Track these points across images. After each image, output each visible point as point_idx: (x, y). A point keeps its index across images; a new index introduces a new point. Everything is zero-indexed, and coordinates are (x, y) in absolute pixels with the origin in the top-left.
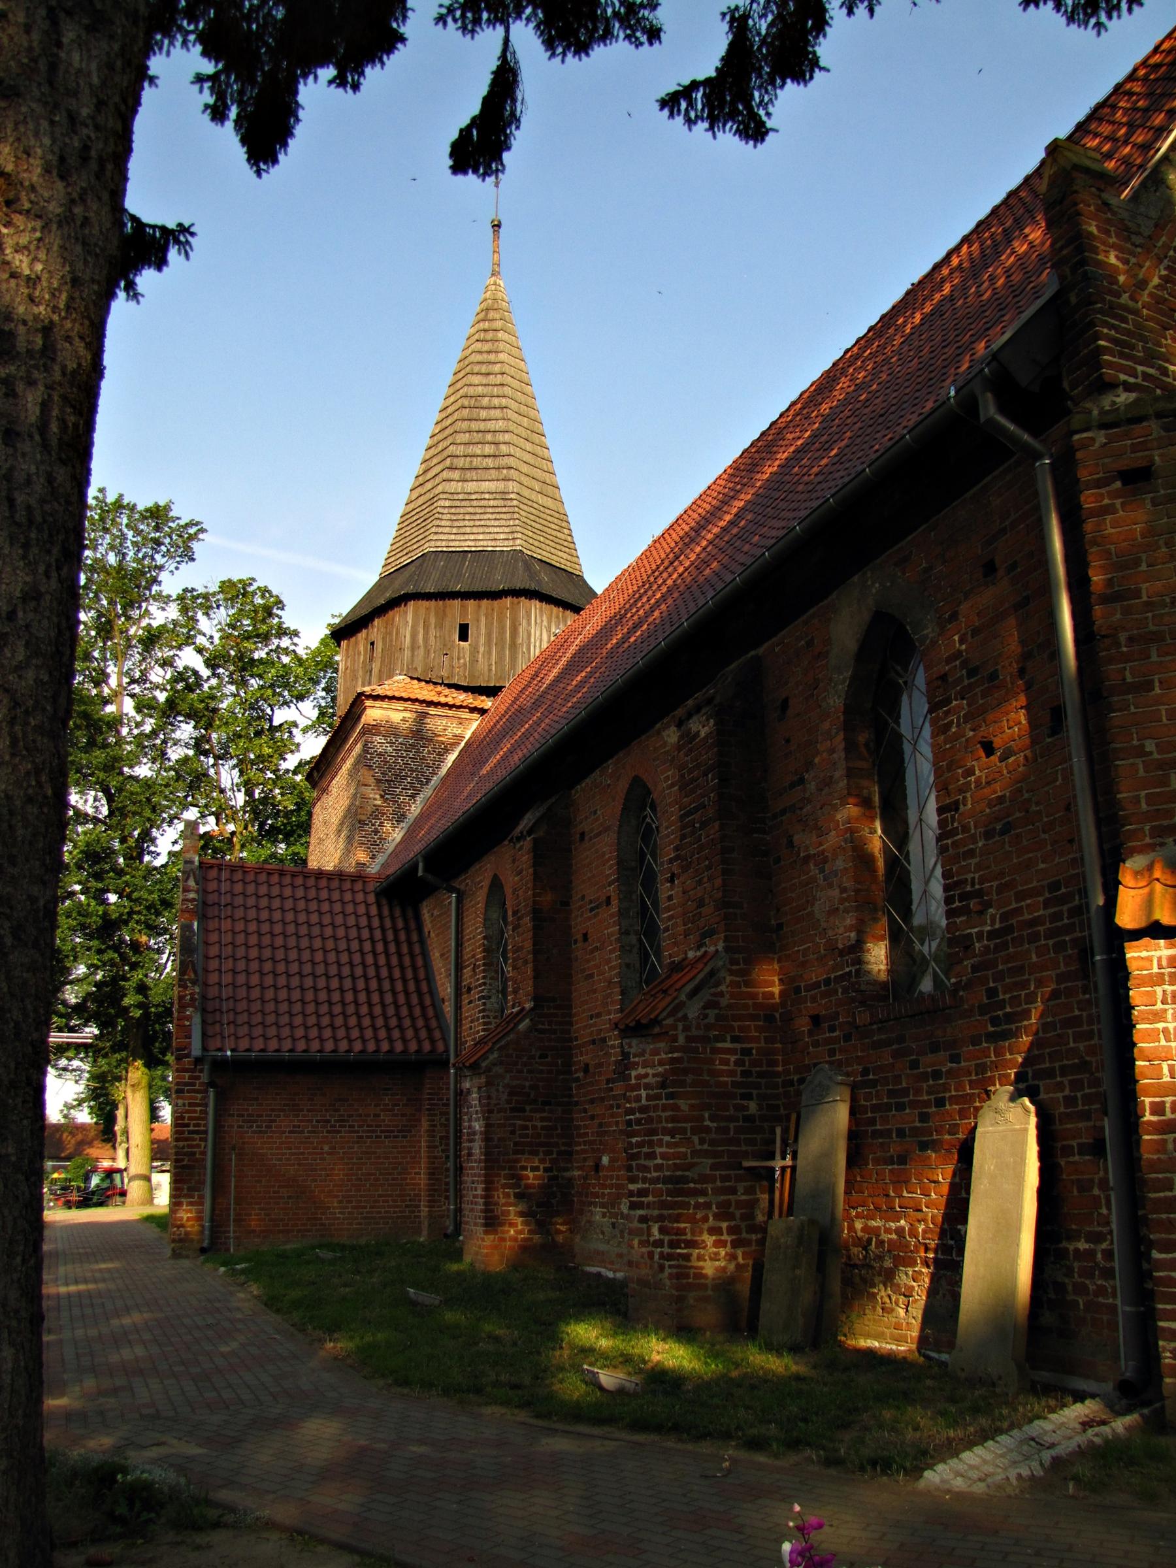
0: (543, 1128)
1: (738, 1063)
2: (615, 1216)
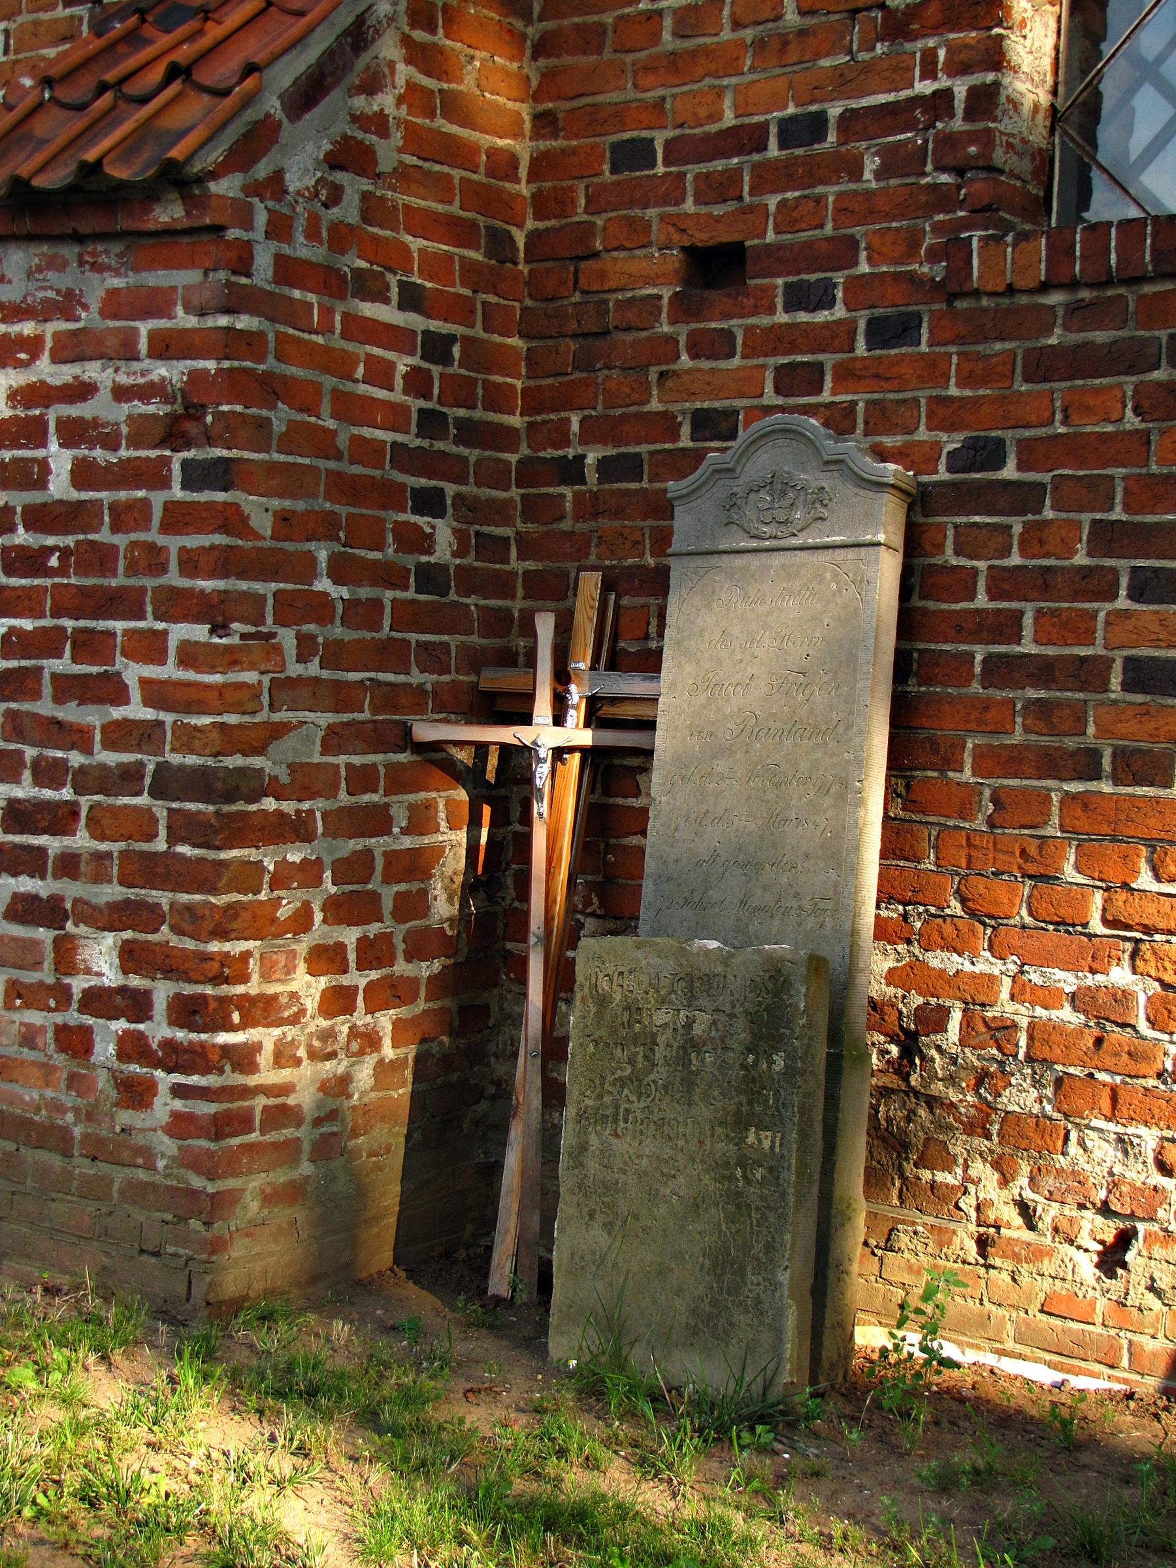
1: (417, 383)
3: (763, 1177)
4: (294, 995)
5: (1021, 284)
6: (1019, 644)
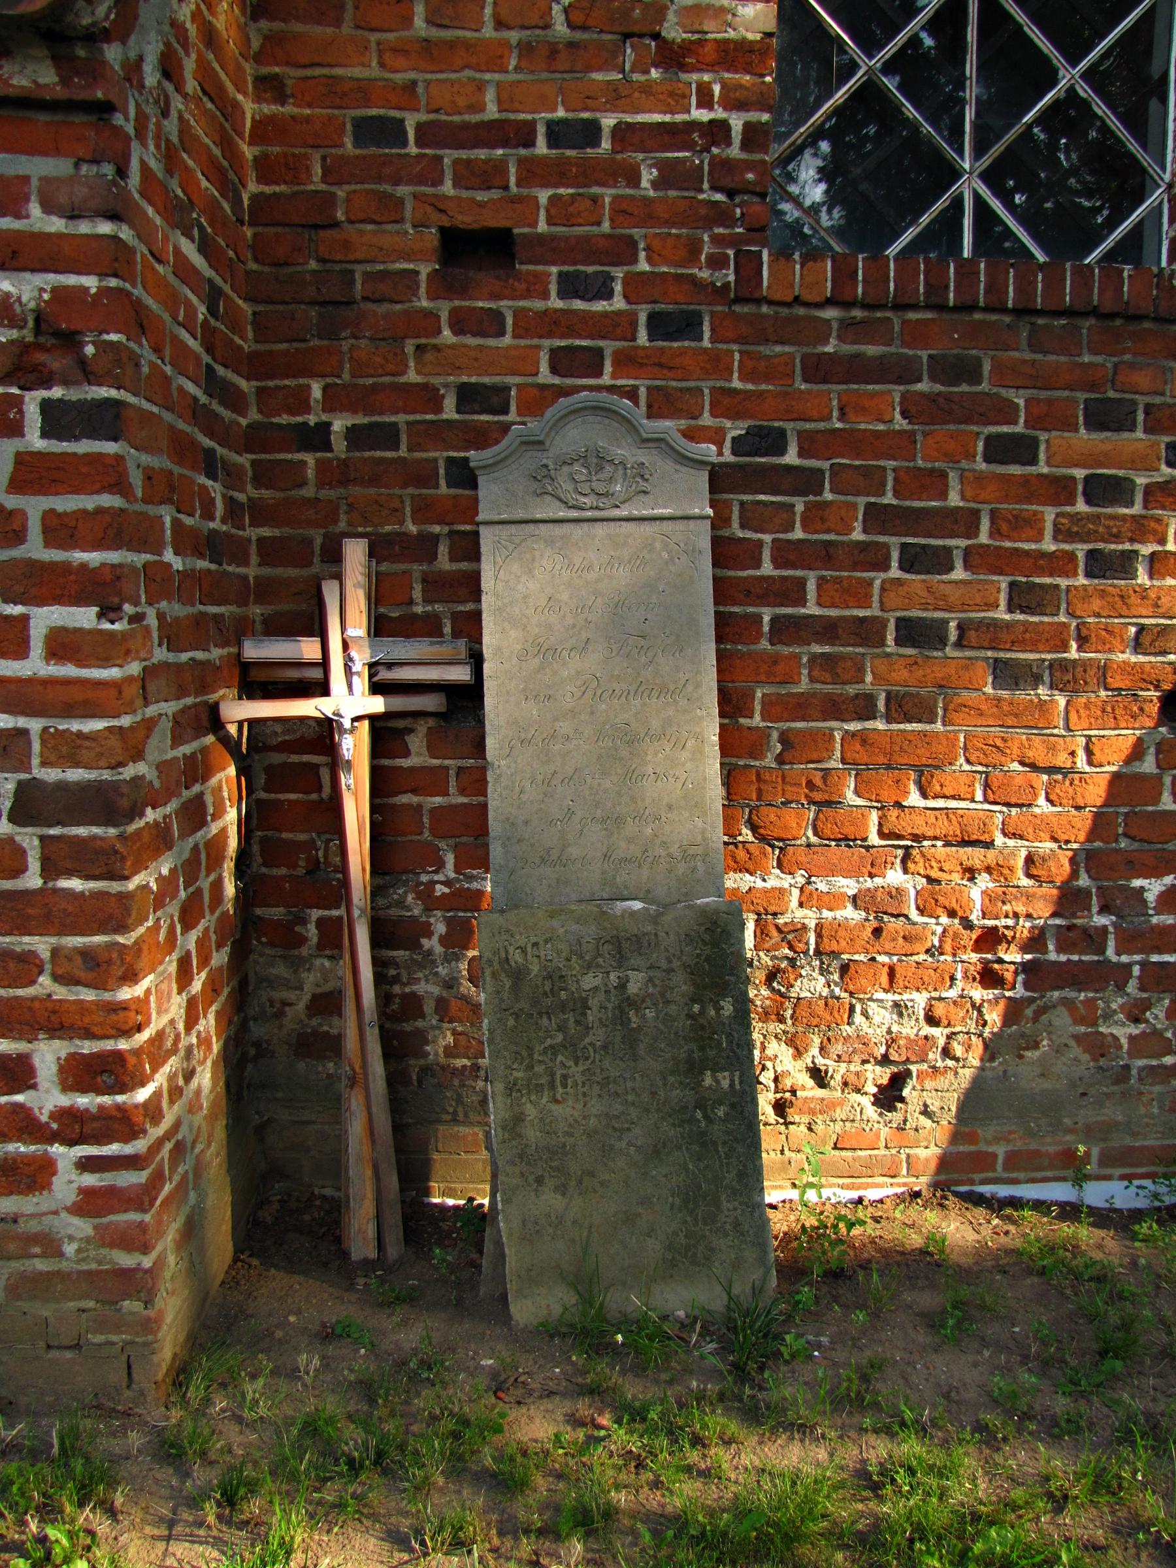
3: (726, 1114)
5: (807, 297)
6: (804, 606)
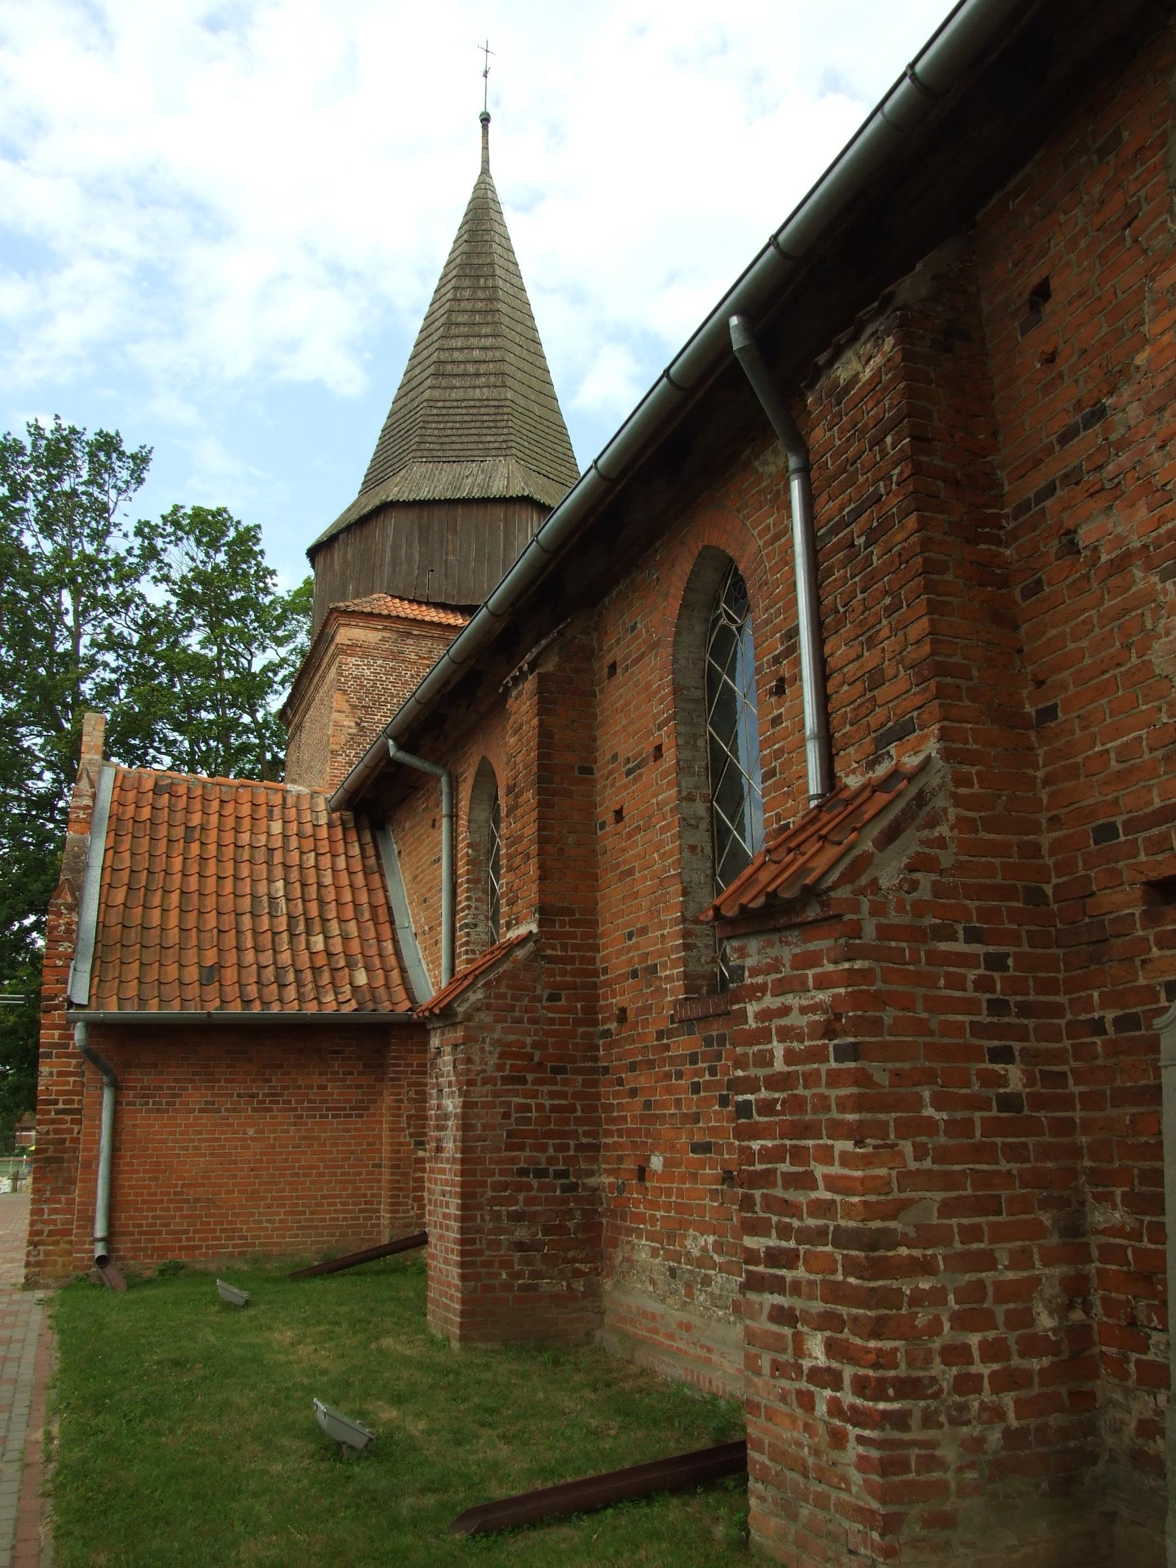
0: (554, 1109)
1: (983, 984)
2: (676, 1256)
4: (933, 1380)
